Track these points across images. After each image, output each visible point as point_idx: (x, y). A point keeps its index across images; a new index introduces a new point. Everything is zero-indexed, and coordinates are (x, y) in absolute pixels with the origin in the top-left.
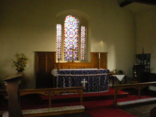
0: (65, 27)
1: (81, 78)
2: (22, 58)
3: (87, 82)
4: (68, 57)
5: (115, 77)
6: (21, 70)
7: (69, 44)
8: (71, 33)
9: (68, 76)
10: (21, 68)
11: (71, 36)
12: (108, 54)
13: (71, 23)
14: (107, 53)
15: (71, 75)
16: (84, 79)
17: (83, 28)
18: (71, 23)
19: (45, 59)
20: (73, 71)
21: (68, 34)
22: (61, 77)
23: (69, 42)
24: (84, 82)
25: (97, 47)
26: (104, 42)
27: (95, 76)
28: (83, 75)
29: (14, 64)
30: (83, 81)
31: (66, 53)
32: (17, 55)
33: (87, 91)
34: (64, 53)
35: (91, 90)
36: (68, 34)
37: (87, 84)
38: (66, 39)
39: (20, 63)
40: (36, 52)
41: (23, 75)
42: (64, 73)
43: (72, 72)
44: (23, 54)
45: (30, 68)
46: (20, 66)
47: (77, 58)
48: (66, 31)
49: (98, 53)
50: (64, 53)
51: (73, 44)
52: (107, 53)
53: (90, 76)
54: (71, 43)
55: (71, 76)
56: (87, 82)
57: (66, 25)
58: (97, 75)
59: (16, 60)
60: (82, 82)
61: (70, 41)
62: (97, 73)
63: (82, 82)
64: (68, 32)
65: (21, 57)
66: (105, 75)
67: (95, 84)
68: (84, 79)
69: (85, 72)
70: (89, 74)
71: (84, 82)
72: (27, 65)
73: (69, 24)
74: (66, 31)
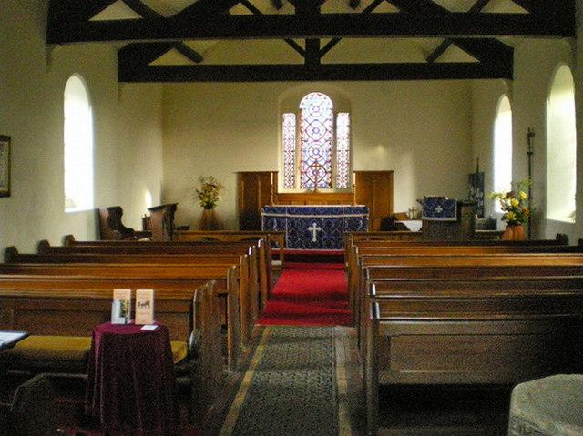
0: (302, 118)
1: (309, 222)
2: (210, 185)
3: (319, 229)
4: (310, 182)
5: (402, 224)
6: (209, 206)
7: (311, 153)
8: (316, 131)
9: (283, 218)
10: (207, 203)
11: (316, 136)
12: (394, 174)
13: (316, 109)
14: (392, 172)
15: (288, 215)
16: (315, 224)
17: (343, 119)
18: (316, 109)
19: (256, 185)
20: (292, 209)
21: (310, 132)
22: (270, 218)
23: (311, 150)
24: (314, 229)
25: (375, 159)
26: (385, 145)
27: (336, 218)
28: (311, 216)
29: (197, 195)
30: (312, 226)
31: (306, 173)
32: (202, 180)
33: (321, 247)
34: (302, 173)
35: (329, 246)
36: (310, 132)
37: (319, 234)
38: (305, 144)
39: (208, 194)
40: (239, 173)
41: (213, 214)
42: (275, 212)
43: (291, 211)
44: (211, 178)
45: (227, 204)
46: (206, 200)
47: (330, 184)
48: (305, 128)
49: (270, 173)
50: (302, 173)
51: (321, 153)
52: (392, 172)
53: (326, 218)
54: (316, 152)
55: (288, 218)
56: (319, 229)
57: (305, 114)
58: (342, 216)
59: (200, 189)
60: (310, 229)
61: (314, 147)
62: (341, 213)
63: (310, 229)
64: (310, 129)
65: (208, 182)
66: (359, 218)
67: (336, 234)
68: (315, 224)
69: (315, 211)
70: (324, 214)
71: (314, 229)
72: (220, 197)
73: (311, 111)
74: (305, 128)
